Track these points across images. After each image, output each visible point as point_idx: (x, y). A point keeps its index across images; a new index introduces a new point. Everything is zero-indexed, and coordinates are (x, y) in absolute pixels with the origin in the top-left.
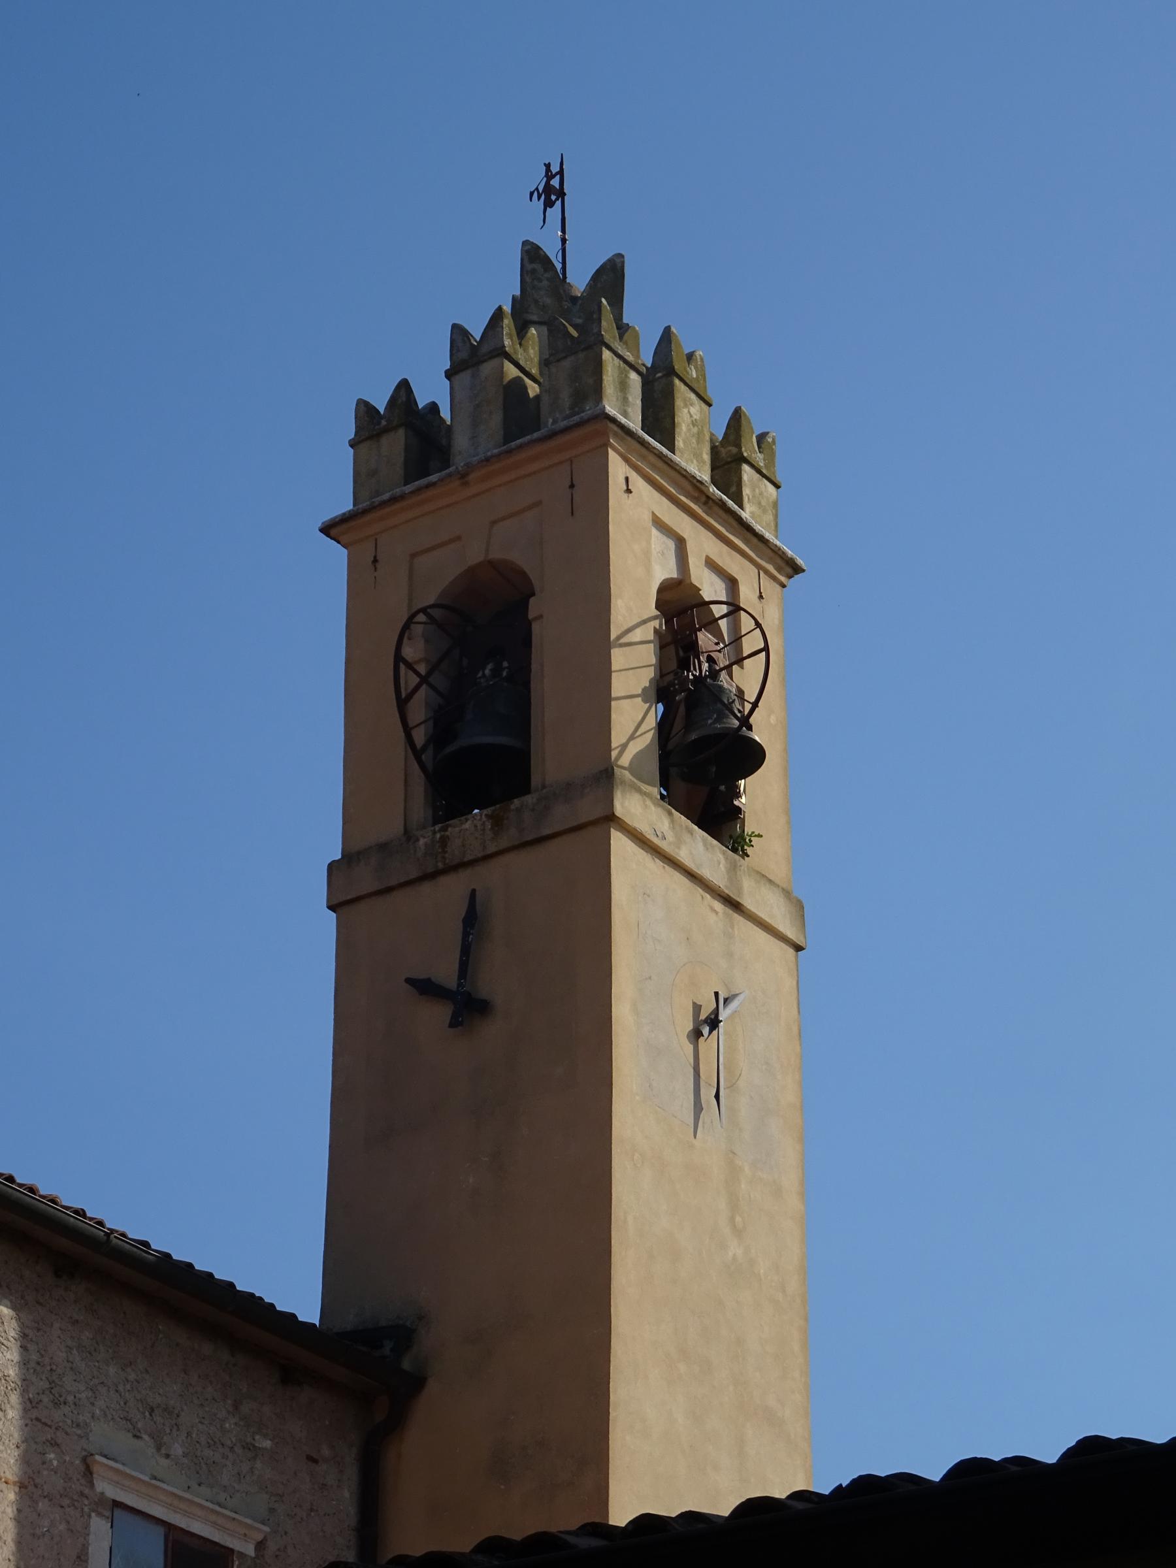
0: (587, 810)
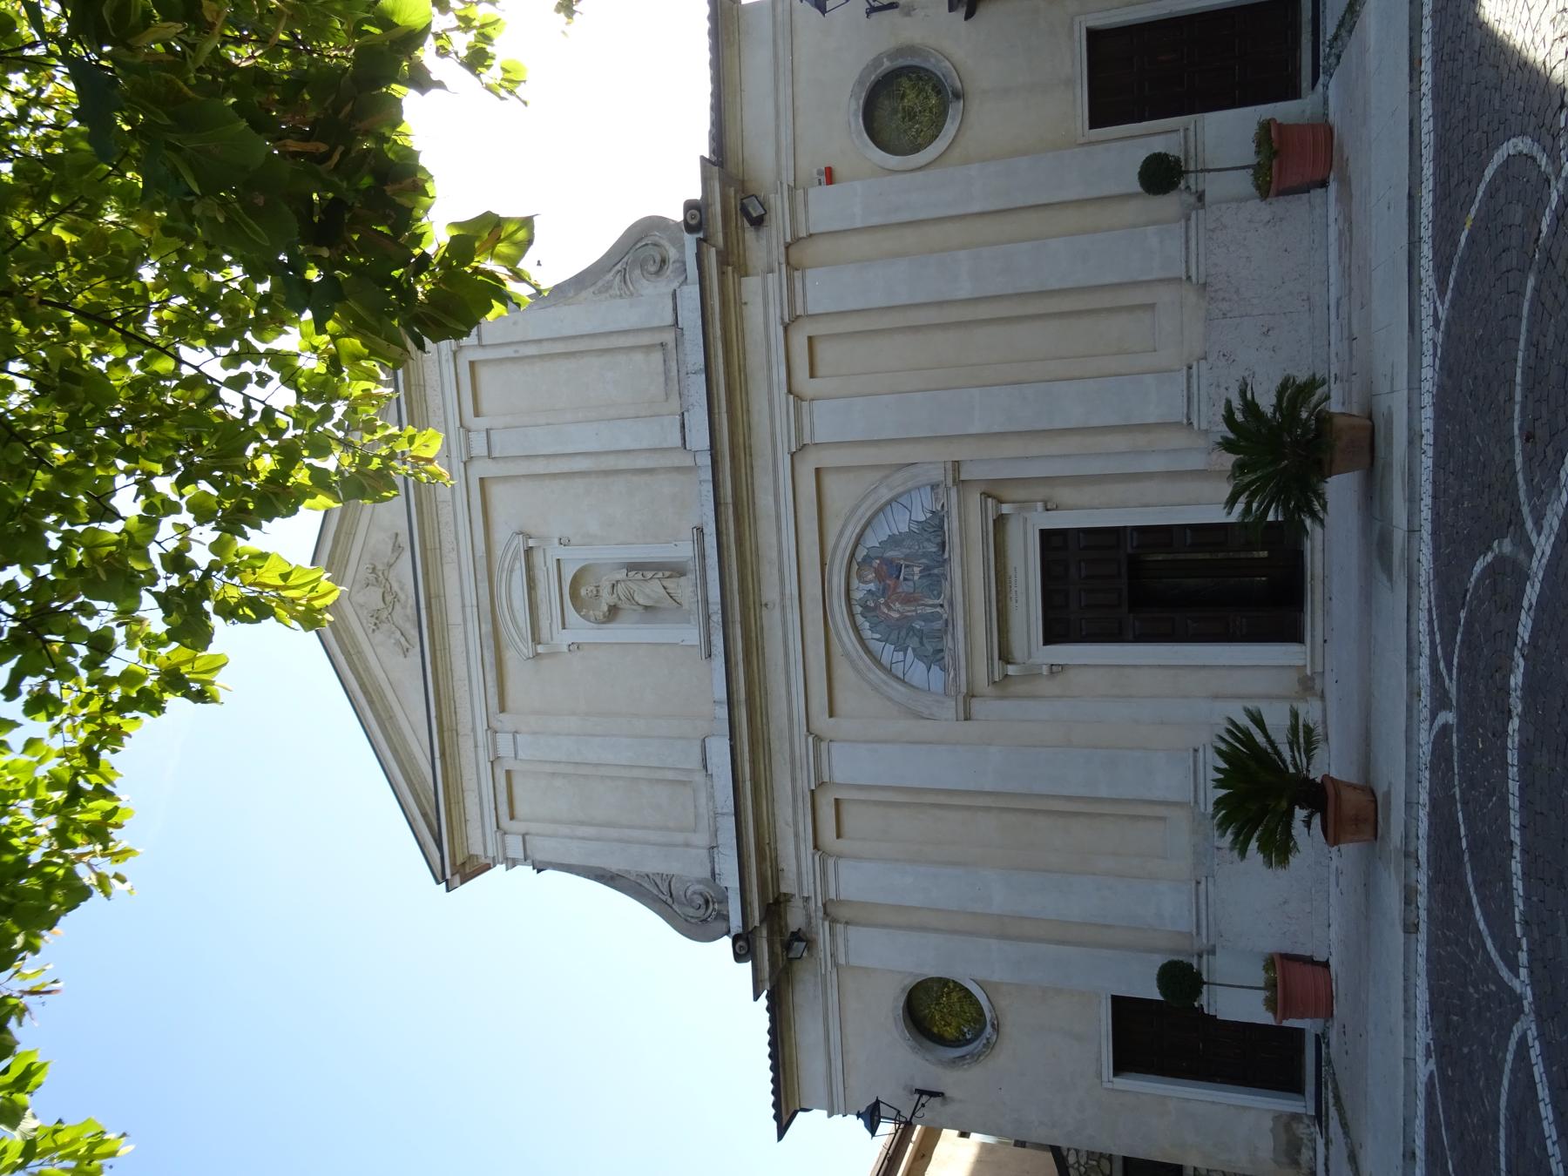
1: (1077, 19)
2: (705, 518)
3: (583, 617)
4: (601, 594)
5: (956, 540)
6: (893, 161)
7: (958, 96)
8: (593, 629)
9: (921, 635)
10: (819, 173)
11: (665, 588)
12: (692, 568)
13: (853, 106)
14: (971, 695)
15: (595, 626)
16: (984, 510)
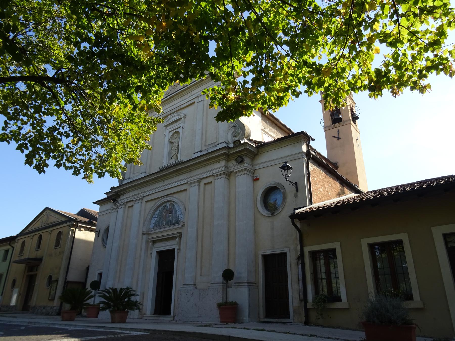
0: (348, 122)
1: (289, 249)
5: (175, 227)
6: (259, 197)
7: (272, 214)
9: (159, 221)
10: (257, 176)
13: (273, 183)
14: (149, 235)
16: (176, 234)
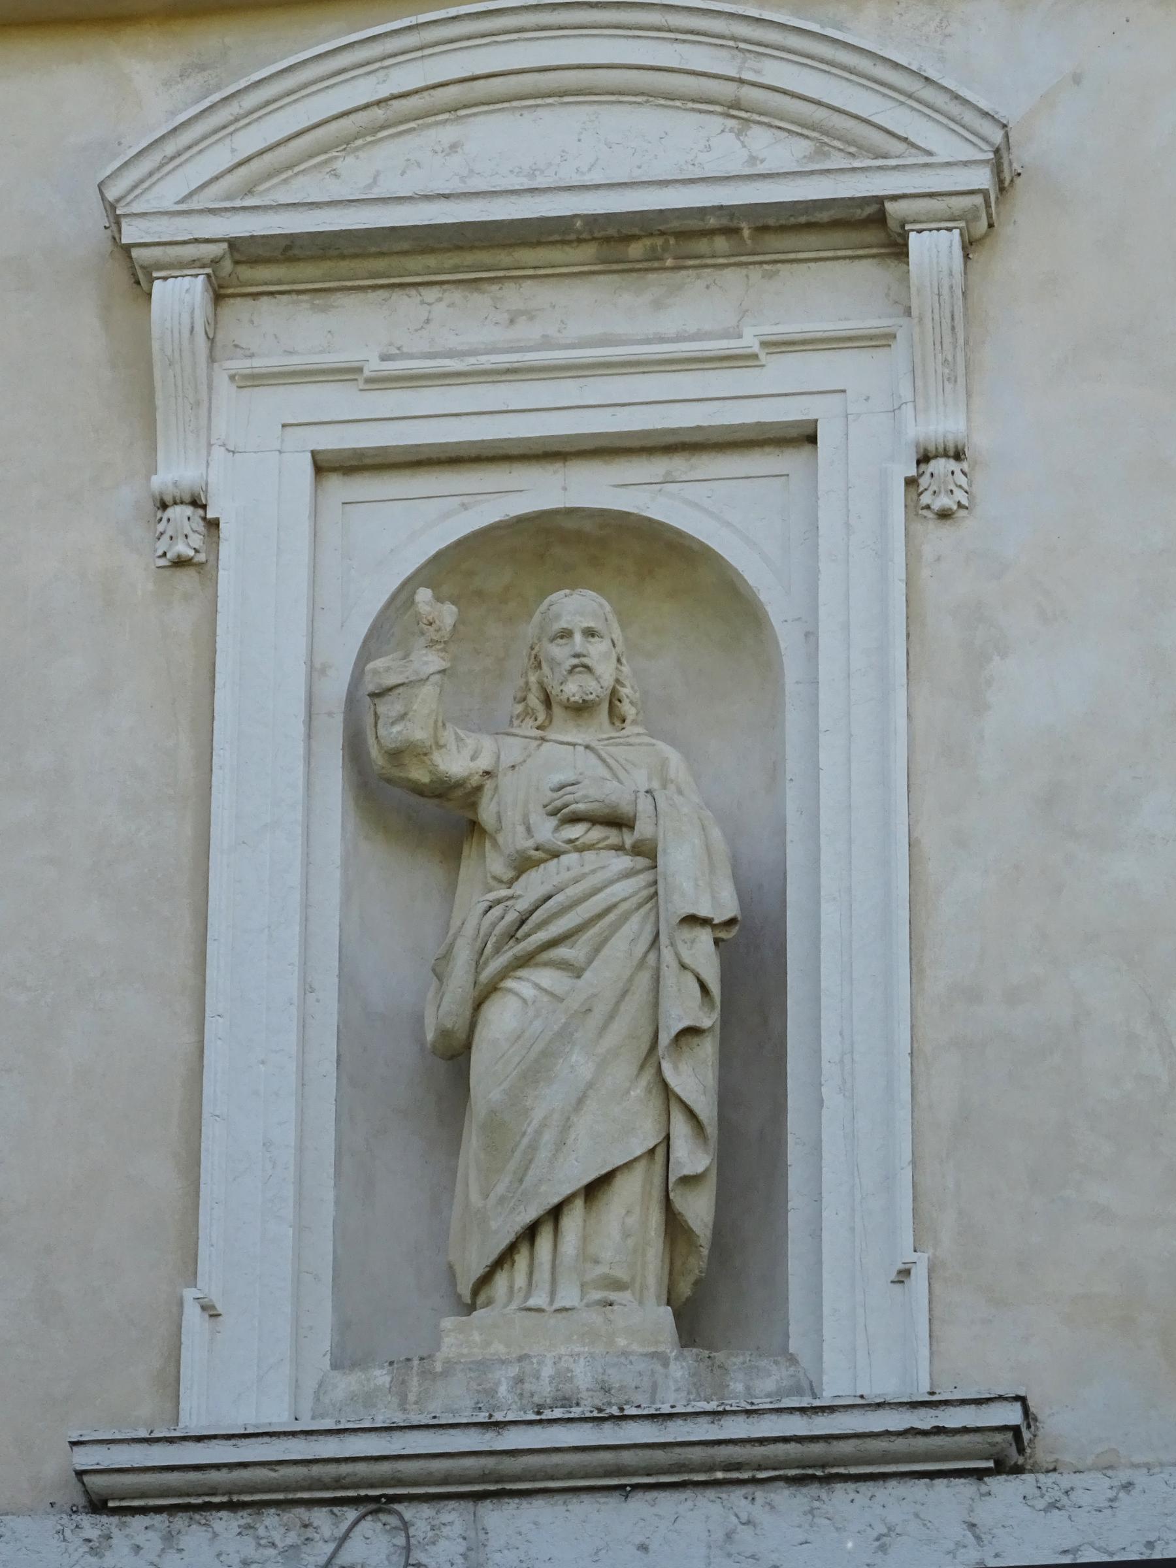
2: (1100, 1486)
3: (402, 598)
4: (567, 731)
8: (315, 671)
11: (595, 1189)
12: (737, 1391)
15: (336, 687)
